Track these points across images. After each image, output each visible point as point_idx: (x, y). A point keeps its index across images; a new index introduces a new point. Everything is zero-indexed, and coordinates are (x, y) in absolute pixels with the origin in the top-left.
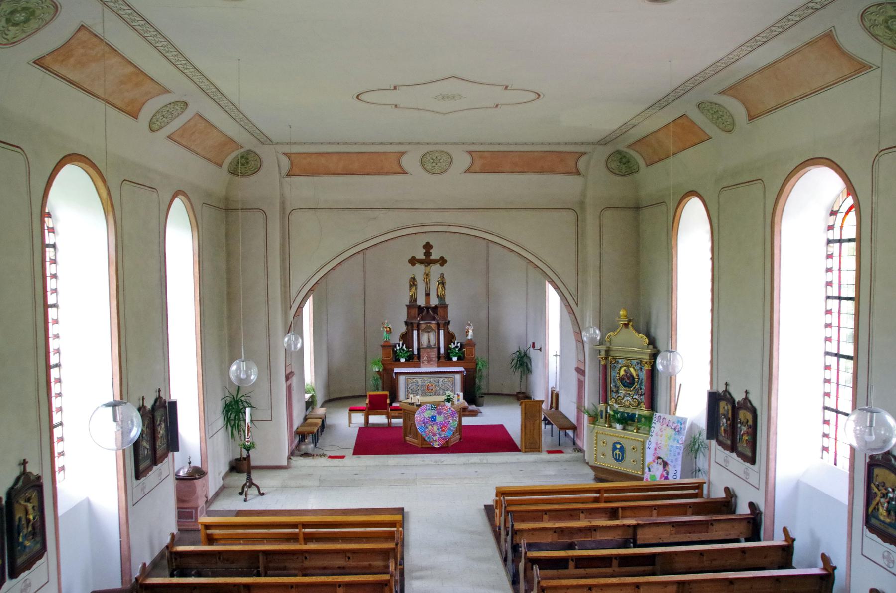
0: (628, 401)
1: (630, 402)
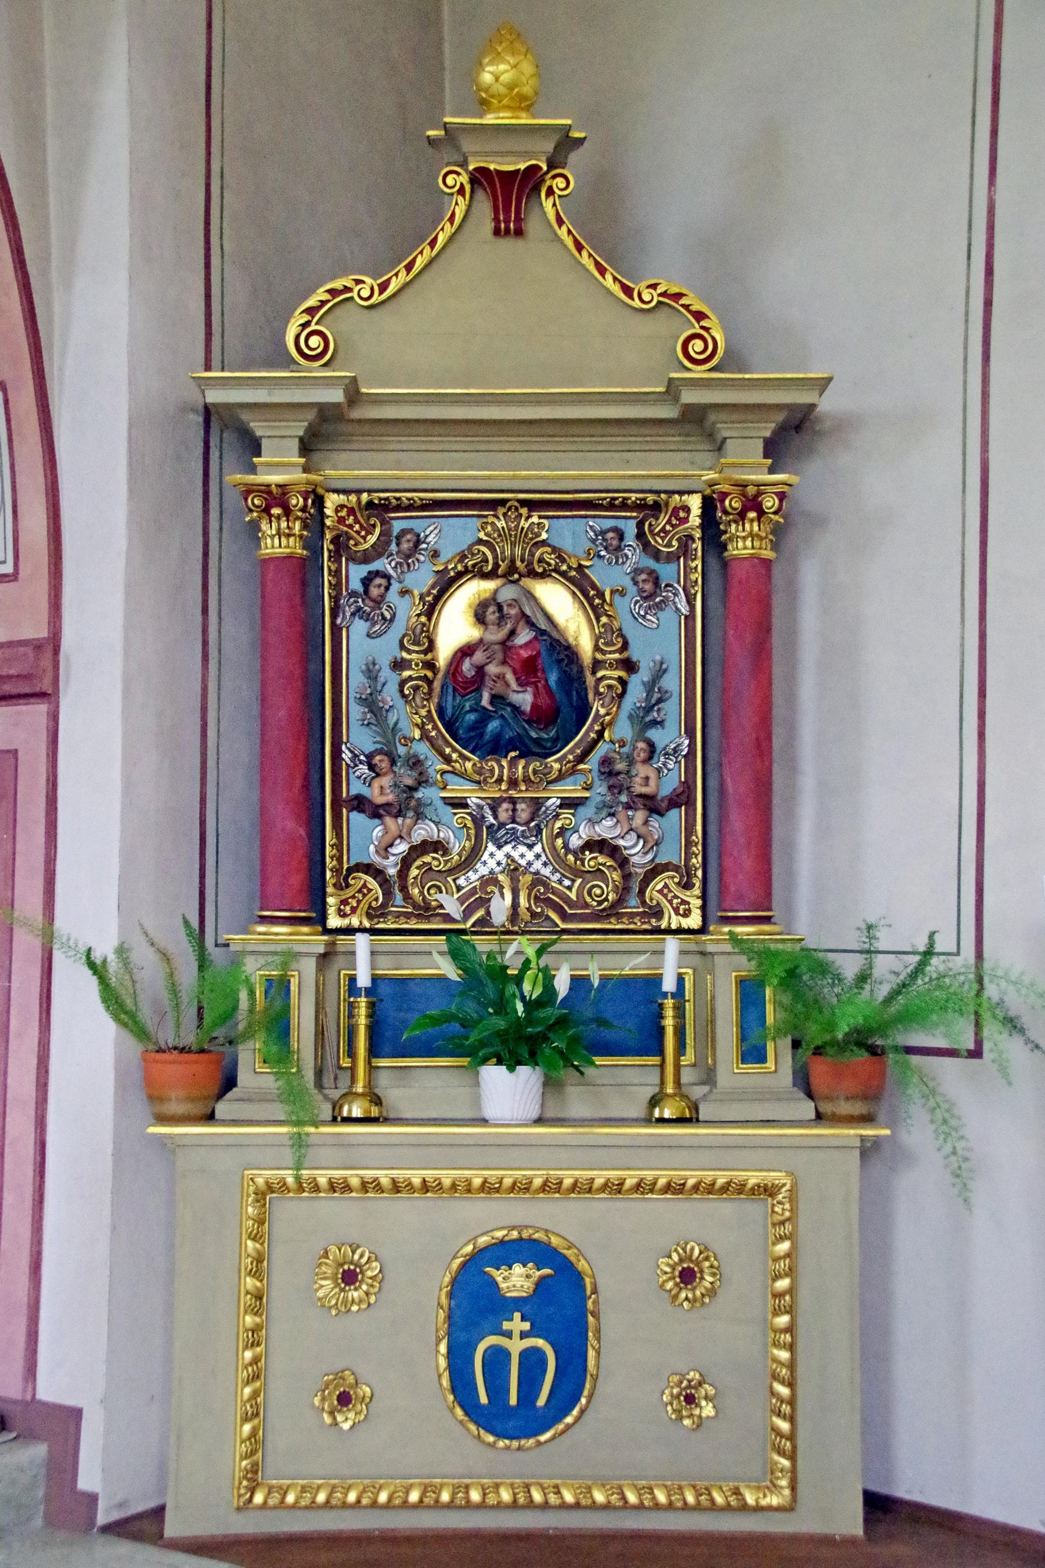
0: (514, 870)
1: (538, 880)
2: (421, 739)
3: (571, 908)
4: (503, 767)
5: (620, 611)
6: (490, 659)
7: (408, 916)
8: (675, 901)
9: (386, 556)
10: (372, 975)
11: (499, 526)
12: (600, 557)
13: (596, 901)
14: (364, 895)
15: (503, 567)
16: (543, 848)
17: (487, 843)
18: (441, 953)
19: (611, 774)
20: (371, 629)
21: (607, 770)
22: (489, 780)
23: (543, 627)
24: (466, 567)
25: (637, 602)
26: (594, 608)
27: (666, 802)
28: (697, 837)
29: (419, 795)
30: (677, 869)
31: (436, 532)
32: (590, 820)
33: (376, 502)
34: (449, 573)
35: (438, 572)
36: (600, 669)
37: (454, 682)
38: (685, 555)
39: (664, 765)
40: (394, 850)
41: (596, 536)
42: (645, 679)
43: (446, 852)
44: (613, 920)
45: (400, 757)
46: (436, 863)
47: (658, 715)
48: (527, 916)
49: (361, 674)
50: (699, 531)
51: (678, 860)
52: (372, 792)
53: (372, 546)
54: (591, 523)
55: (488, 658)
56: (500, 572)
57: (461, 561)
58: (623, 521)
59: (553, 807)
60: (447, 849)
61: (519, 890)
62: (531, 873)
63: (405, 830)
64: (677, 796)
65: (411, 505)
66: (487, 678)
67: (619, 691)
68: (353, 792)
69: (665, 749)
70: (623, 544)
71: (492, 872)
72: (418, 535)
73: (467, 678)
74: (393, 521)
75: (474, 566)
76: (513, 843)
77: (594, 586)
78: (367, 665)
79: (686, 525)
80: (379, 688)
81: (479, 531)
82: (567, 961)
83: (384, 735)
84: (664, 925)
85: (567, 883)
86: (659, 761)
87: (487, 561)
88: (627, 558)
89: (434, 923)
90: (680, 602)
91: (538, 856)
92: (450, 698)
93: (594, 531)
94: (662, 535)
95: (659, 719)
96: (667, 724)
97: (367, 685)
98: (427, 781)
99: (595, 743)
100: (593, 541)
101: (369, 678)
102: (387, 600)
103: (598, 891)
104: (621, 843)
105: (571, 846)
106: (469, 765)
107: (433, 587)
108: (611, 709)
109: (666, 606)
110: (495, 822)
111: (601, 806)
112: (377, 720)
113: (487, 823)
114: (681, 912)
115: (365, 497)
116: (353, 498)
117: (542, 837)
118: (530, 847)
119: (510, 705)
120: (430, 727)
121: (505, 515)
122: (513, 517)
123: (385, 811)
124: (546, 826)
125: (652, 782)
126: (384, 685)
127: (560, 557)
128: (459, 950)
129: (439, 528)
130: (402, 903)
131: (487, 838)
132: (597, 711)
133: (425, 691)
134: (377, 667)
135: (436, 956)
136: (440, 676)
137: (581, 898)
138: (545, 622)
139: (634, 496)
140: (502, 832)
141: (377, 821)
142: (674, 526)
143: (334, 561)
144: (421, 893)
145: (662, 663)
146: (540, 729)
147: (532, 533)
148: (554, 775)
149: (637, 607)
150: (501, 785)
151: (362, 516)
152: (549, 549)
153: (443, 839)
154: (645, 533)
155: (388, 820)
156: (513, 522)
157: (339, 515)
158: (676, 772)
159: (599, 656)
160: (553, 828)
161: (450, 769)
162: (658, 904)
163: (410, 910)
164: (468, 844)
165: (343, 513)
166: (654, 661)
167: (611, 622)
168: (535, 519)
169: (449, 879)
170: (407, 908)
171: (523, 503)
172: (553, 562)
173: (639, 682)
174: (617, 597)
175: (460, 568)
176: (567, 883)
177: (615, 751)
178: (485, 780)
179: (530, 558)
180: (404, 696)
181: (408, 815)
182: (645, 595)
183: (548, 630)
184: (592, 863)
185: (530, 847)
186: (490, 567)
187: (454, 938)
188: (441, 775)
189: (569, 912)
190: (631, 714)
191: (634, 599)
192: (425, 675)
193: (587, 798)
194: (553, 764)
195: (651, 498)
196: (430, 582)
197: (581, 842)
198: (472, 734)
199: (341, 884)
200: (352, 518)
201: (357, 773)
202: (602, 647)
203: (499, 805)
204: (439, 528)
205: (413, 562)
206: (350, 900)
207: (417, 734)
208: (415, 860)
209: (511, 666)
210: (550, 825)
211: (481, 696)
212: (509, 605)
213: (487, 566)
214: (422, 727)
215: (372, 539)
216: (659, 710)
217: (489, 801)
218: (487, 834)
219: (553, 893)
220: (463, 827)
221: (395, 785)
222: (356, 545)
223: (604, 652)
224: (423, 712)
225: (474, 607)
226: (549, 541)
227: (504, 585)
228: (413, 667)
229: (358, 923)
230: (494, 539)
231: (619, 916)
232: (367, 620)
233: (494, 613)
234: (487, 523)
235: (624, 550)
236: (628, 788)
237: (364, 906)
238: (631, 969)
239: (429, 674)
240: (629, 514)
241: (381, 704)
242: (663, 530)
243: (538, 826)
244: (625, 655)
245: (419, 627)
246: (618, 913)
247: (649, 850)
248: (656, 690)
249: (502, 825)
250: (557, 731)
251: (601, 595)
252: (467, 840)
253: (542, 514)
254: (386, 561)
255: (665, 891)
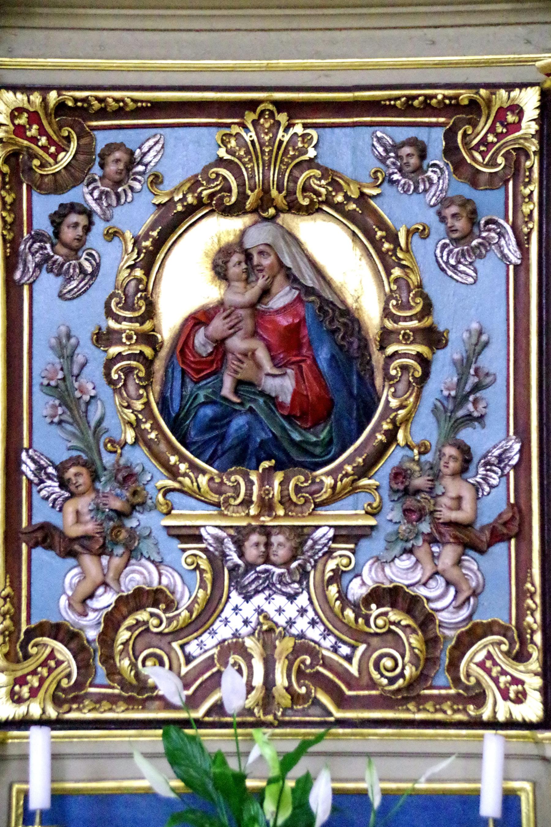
2: (136, 442)
3: (350, 687)
4: (252, 483)
5: (419, 259)
6: (234, 328)
7: (113, 700)
8: (503, 679)
9: (85, 182)
10: (53, 790)
11: (248, 139)
12: (392, 182)
13: (386, 677)
14: (51, 671)
15: (252, 197)
16: (310, 599)
17: (229, 592)
18: (149, 756)
19: (406, 492)
20: (64, 287)
21: (401, 487)
22: (232, 501)
23: (310, 284)
24: (199, 198)
25: (445, 246)
26: (382, 255)
27: (487, 533)
28: (533, 585)
29: (132, 523)
30: (504, 631)
31: (158, 147)
32: (378, 559)
33: (70, 104)
34: (175, 208)
35: (159, 206)
36: (390, 344)
37: (183, 362)
38: (516, 176)
39: (483, 479)
40: (95, 604)
41: (386, 150)
42: (457, 357)
43: (171, 605)
44: (411, 706)
45: (105, 469)
46: (155, 621)
47: (476, 408)
48: (286, 700)
49: (50, 352)
50: (535, 141)
51: (506, 618)
52: (64, 518)
53: (65, 168)
54: (379, 134)
55: (230, 329)
56: (248, 205)
57: (191, 190)
58: (425, 130)
59: (324, 541)
60: (173, 601)
61: (274, 662)
62: (293, 636)
63: (111, 575)
64: (505, 524)
65: (121, 109)
66: (230, 356)
67: (418, 374)
68: (37, 520)
69: (485, 456)
70: (425, 163)
71: (236, 635)
72: (132, 153)
73: (201, 356)
74: (96, 133)
75: (211, 196)
76: (267, 592)
77: (382, 224)
78: (59, 338)
79: (517, 134)
80: (75, 371)
81: (220, 147)
82: (327, 766)
83: (83, 439)
84: (486, 714)
85: (345, 650)
86: (477, 473)
87: (229, 190)
88: (431, 184)
89: (150, 710)
90: (508, 245)
91: (302, 612)
92: (177, 384)
93: (384, 145)
94: (482, 148)
95: (476, 414)
96: (488, 420)
97: (59, 367)
98: (143, 504)
99: (383, 448)
100: (383, 160)
101: (61, 356)
102: (87, 245)
103: (388, 663)
104: (422, 592)
105: (350, 597)
106: (203, 480)
107: (152, 228)
108: (406, 399)
109: (487, 251)
110: (240, 562)
111: (394, 538)
112: (73, 417)
113: (230, 564)
114: (512, 695)
115: (53, 96)
116: (36, 98)
117: (308, 583)
118: (292, 597)
119: (262, 393)
120: (148, 426)
121: (255, 123)
122: (267, 125)
123: (83, 547)
124: (314, 567)
125: (467, 505)
126: (83, 366)
127: (334, 183)
128: (181, 750)
129: (161, 142)
130: (107, 681)
131: (230, 586)
132: (387, 402)
133: (142, 374)
134: (73, 341)
135: (140, 762)
136: (163, 353)
137: (364, 673)
138: (312, 275)
139: (440, 93)
140: (252, 576)
141: (71, 561)
142: (499, 136)
143: (11, 189)
144: (133, 665)
145: (480, 333)
146: (307, 429)
147: (294, 149)
148: (325, 495)
149: (445, 253)
150: (248, 508)
151: (50, 123)
152: (318, 173)
153: (167, 587)
154: (458, 148)
155: (88, 560)
156: (266, 134)
157: (17, 122)
158: (502, 489)
159: (389, 325)
160: (324, 572)
161: (177, 485)
162: (478, 683)
163: (117, 691)
164: (201, 593)
165: (22, 120)
166: (469, 331)
167: (407, 275)
168: (298, 129)
169: (175, 645)
170: (113, 688)
171: (281, 106)
172: (323, 191)
173: (448, 361)
174: (416, 240)
175: (190, 199)
176: (345, 650)
177: (414, 460)
178: (226, 501)
179: (291, 185)
180: (111, 382)
181: (115, 552)
182: (455, 235)
183: (317, 287)
184: (380, 622)
185: (292, 597)
186: (234, 199)
187: (173, 731)
188: (164, 495)
189: (349, 693)
190: (436, 407)
191: (441, 243)
192: (141, 353)
193: (372, 528)
194: (323, 478)
195: (465, 96)
196: (150, 220)
197: (364, 591)
198: (207, 437)
199: (17, 653)
200: (35, 127)
201: (44, 493)
202: (394, 311)
203: (246, 537)
204: (161, 142)
205: (125, 190)
206: (29, 678)
207: (130, 435)
208: (125, 618)
209: (264, 339)
210: (320, 566)
211: (222, 381)
212: (261, 253)
213: (230, 197)
214: (136, 426)
215: (65, 158)
216: (475, 402)
217: (232, 532)
218: (230, 580)
219: (324, 665)
220: (195, 569)
221: (98, 509)
222: (42, 166)
223: (396, 319)
224: (138, 405)
225: (212, 254)
226: (319, 161)
227: (255, 223)
228: (124, 340)
229: (40, 712)
230: (240, 158)
231: (421, 700)
232: (58, 275)
233: (239, 263)
234: (230, 135)
235: (426, 172)
236: (432, 513)
237: (50, 686)
238: (429, 781)
239: (148, 351)
240: (434, 120)
241: (78, 394)
242: (484, 141)
243: (302, 567)
244: (427, 322)
245: (133, 283)
246: (419, 695)
247: (463, 603)
248: (472, 372)
249: (250, 566)
250: (330, 432)
251: (393, 237)
252: (200, 587)
253: (309, 121)
254: (86, 190)
255: (489, 664)
